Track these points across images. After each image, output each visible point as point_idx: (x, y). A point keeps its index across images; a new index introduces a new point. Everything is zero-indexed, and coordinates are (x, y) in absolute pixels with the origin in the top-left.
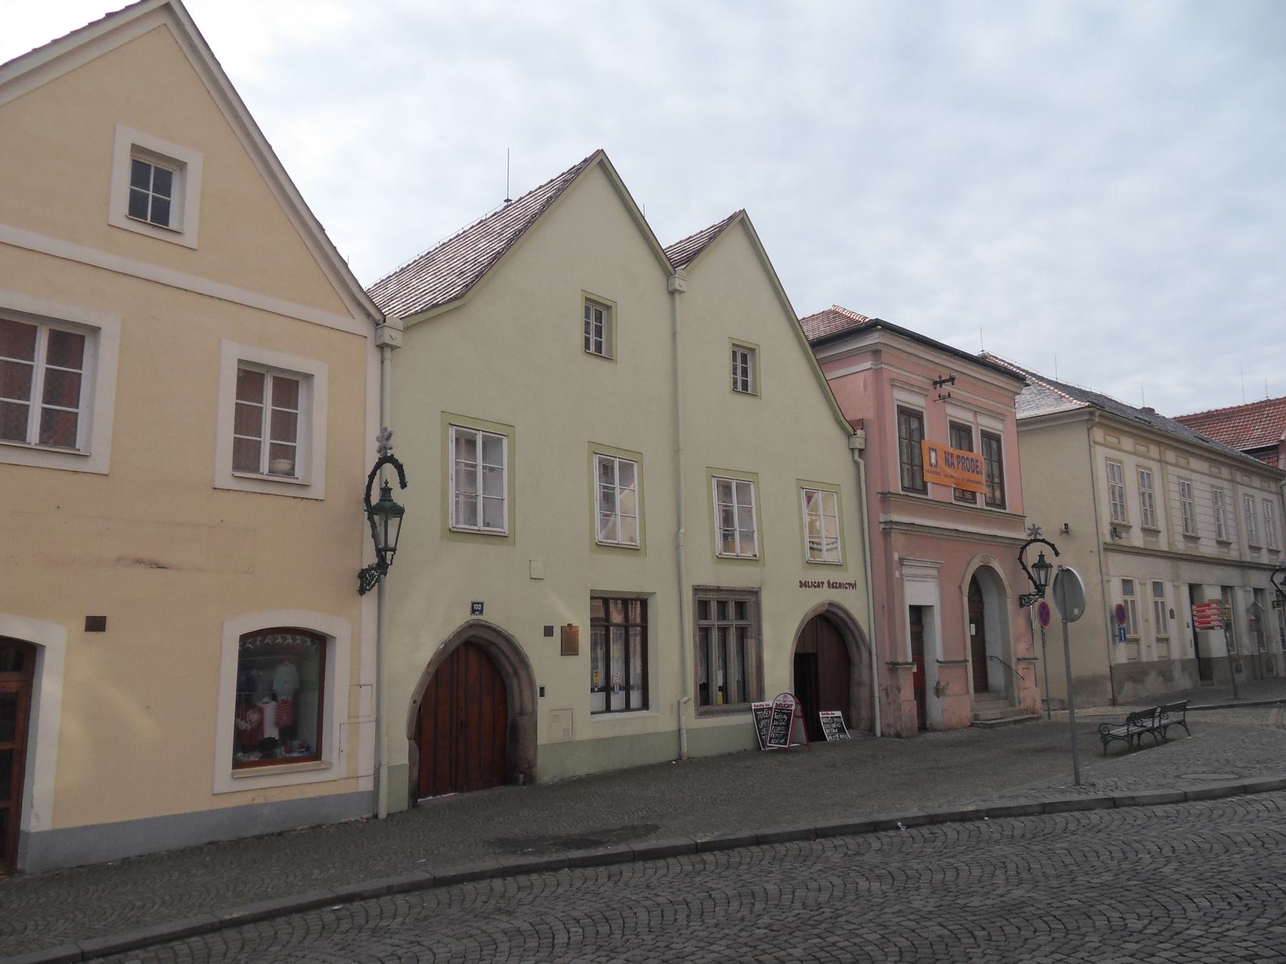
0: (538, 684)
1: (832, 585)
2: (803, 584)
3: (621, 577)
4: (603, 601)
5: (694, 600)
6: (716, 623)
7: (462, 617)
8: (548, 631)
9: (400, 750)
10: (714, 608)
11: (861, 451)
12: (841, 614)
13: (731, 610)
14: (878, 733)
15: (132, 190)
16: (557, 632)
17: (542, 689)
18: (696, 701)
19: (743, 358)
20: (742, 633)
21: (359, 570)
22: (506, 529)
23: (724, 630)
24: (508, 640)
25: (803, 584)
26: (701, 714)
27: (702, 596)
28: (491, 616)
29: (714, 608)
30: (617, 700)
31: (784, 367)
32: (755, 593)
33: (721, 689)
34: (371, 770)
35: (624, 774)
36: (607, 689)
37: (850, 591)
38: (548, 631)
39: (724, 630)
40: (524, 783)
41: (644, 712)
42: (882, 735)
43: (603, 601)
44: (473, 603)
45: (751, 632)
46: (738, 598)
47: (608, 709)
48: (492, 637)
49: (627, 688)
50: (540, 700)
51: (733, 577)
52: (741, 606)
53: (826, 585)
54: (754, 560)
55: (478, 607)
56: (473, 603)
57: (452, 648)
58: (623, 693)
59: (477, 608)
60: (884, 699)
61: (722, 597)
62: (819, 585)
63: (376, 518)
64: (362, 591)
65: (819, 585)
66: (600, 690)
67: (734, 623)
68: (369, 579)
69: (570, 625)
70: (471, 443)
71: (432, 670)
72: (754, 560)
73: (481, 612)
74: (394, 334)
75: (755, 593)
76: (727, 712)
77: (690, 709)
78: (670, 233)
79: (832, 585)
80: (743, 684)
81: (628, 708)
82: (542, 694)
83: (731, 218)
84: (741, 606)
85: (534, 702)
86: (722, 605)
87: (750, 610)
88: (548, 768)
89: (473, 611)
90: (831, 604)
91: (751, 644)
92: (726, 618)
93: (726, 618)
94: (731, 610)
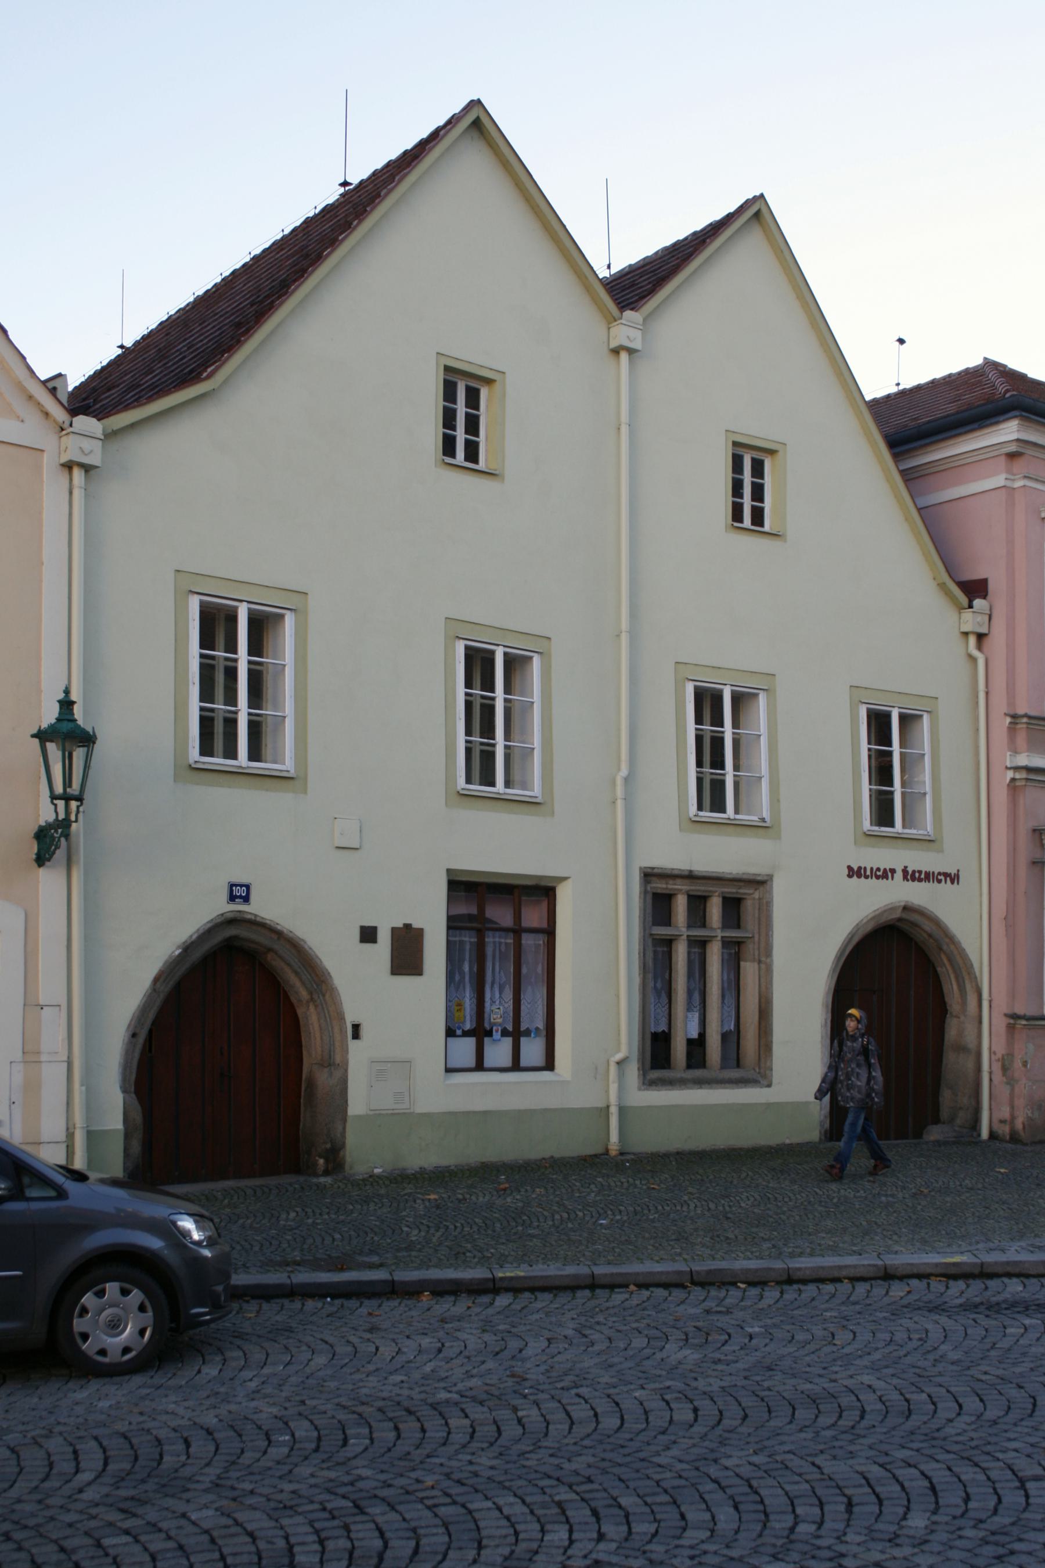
0: (350, 1019)
1: (910, 876)
2: (854, 872)
3: (500, 846)
4: (464, 888)
5: (645, 892)
6: (720, 934)
7: (219, 906)
8: (368, 935)
9: (113, 1110)
10: (681, 905)
11: (981, 637)
12: (927, 926)
13: (715, 910)
14: (985, 1134)
15: (445, 407)
16: (384, 937)
17: (356, 1028)
18: (642, 1060)
19: (749, 470)
20: (735, 952)
21: (36, 829)
22: (536, 791)
23: (699, 945)
24: (295, 946)
25: (854, 872)
26: (649, 1083)
27: (660, 886)
28: (263, 906)
29: (681, 905)
30: (499, 1051)
31: (838, 487)
32: (760, 883)
33: (690, 1042)
34: (62, 1136)
35: (485, 1172)
36: (481, 1033)
37: (946, 887)
38: (368, 935)
39: (699, 945)
40: (326, 1173)
41: (546, 1075)
42: (992, 1135)
43: (464, 888)
44: (232, 886)
45: (750, 948)
46: (731, 890)
47: (480, 1066)
48: (262, 939)
49: (516, 1034)
50: (353, 1044)
51: (719, 854)
52: (733, 907)
53: (899, 875)
54: (761, 828)
55: (237, 891)
56: (232, 886)
57: (197, 954)
58: (508, 1042)
59: (239, 893)
60: (998, 1077)
61: (699, 888)
62: (886, 874)
63: (51, 747)
64: (41, 860)
65: (886, 874)
66: (466, 1034)
67: (720, 934)
68: (49, 843)
69: (407, 926)
70: (488, 659)
71: (165, 989)
72: (761, 828)
73: (246, 899)
74: (87, 444)
75: (760, 883)
76: (700, 1083)
77: (633, 1071)
78: (612, 252)
79: (910, 876)
80: (732, 1039)
81: (516, 1066)
82: (356, 1035)
83: (452, 122)
84: (733, 907)
85: (345, 1051)
86: (698, 904)
87: (749, 908)
88: (364, 1153)
89: (232, 898)
90: (906, 908)
91: (749, 970)
92: (696, 926)
93: (696, 926)
94: (715, 910)
